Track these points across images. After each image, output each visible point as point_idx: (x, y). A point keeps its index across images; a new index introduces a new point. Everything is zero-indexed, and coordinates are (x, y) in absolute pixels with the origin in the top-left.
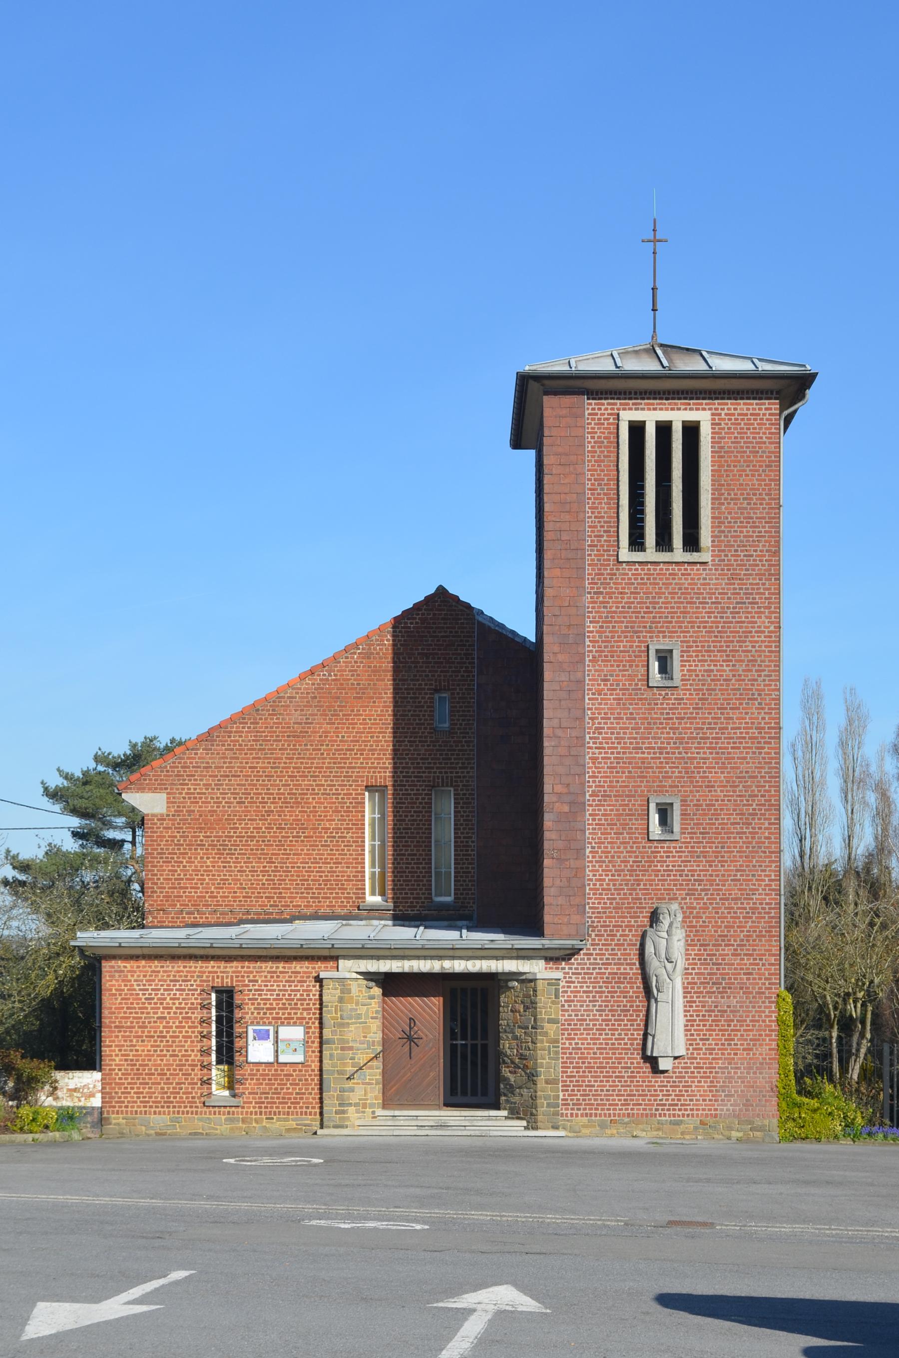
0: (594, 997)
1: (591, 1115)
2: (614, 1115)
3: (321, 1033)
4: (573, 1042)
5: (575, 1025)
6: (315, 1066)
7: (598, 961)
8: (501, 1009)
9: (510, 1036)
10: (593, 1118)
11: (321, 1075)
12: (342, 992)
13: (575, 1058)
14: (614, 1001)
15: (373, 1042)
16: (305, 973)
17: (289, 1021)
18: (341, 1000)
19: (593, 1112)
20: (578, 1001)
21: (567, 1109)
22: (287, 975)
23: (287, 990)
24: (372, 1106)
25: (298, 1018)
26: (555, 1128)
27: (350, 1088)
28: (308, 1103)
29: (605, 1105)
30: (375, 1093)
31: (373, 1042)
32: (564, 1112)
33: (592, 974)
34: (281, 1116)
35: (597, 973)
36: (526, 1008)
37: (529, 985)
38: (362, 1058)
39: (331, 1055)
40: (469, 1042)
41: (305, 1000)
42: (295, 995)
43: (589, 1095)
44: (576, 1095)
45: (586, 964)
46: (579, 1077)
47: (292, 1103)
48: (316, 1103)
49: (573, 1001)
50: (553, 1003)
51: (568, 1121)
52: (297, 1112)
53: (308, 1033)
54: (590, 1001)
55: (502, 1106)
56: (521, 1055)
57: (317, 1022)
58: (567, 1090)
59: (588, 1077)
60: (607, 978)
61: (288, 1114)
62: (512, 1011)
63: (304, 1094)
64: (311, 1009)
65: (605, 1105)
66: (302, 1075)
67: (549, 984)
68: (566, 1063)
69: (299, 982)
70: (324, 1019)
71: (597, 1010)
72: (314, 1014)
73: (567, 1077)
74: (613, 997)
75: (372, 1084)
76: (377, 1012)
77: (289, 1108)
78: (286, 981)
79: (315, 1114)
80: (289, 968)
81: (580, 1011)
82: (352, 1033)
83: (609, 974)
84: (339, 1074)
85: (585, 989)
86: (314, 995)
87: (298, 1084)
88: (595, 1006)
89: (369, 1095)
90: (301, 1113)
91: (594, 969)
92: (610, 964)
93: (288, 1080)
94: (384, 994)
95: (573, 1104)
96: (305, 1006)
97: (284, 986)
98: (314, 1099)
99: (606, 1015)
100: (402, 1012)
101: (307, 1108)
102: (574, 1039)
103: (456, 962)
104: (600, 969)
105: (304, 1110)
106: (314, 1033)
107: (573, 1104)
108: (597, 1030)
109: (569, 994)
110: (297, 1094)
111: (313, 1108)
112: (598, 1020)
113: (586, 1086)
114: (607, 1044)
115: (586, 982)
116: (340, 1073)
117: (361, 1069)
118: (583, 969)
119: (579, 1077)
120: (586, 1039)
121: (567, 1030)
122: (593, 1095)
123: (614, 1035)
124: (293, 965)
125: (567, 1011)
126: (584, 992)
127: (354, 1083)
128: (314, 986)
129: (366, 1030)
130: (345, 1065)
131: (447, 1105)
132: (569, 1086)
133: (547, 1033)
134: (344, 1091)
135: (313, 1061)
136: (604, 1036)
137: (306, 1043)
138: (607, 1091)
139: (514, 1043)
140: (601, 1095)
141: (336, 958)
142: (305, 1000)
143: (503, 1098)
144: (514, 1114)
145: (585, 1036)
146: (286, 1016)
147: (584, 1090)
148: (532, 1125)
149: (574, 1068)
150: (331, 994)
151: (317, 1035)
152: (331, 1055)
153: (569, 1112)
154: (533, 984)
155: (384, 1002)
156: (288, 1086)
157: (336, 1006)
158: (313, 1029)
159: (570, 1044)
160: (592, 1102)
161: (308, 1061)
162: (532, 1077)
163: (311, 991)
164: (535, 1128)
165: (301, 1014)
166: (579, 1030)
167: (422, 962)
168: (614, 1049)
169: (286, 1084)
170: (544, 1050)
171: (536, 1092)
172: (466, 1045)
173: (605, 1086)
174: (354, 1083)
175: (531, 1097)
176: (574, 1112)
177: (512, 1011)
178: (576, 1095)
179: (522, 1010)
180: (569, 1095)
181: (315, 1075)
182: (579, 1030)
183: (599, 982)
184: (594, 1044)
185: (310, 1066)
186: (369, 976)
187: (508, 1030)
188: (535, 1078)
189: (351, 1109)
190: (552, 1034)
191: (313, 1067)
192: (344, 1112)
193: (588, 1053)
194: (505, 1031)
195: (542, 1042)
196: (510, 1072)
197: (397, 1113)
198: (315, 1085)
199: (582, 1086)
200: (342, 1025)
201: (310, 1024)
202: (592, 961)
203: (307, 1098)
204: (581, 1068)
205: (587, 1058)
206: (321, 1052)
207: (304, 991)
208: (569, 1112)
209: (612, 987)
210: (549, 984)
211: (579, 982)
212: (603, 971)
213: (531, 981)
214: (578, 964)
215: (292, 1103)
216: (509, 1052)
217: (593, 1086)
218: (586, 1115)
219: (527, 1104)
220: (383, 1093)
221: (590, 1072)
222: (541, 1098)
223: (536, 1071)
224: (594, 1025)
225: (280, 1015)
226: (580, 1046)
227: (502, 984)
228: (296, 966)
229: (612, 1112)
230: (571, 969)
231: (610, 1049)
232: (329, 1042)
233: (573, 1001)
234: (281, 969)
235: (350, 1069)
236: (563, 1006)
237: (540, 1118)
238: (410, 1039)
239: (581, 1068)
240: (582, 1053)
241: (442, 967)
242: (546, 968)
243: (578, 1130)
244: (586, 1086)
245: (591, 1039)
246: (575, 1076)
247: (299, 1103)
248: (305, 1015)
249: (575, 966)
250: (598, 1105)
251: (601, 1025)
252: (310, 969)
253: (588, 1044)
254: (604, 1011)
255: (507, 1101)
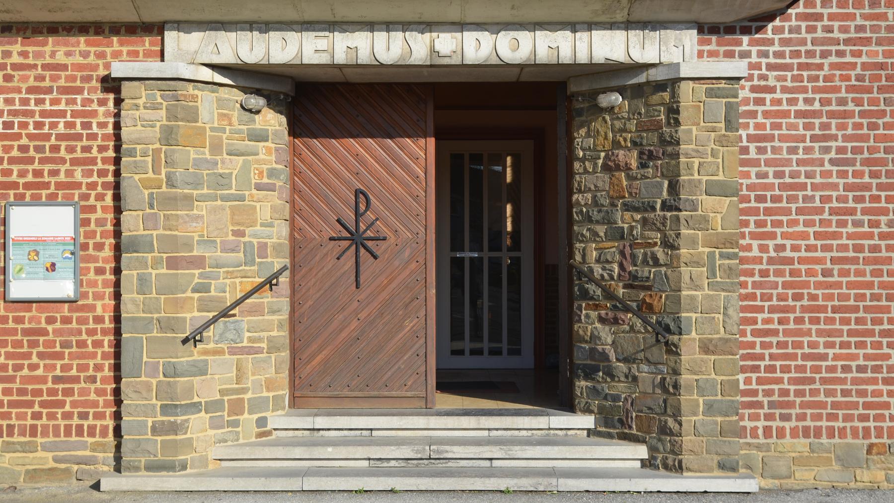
0: (825, 126)
1: (818, 433)
2: (879, 432)
3: (117, 223)
4: (771, 243)
5: (776, 199)
6: (103, 307)
7: (836, 34)
8: (577, 165)
9: (601, 230)
10: (824, 440)
11: (118, 332)
12: (172, 115)
13: (775, 286)
14: (877, 139)
15: (263, 247)
16: (79, 67)
17: (37, 193)
18: (168, 137)
19: (824, 423)
20: (782, 138)
21: (754, 417)
22: (32, 73)
23: (31, 114)
24: (257, 405)
25: (60, 186)
26: (728, 467)
27: (194, 364)
28: (85, 404)
29: (855, 406)
30: (269, 373)
31: (263, 247)
32: (749, 424)
33: (820, 67)
34: (16, 439)
35: (833, 66)
36: (646, 158)
37: (655, 98)
38: (228, 288)
39: (143, 281)
40: (486, 254)
41: (79, 137)
42: (53, 126)
43: (812, 381)
44: (780, 381)
45: (803, 42)
46: (786, 333)
47: (43, 404)
48: (106, 404)
49: (771, 138)
50: (720, 141)
51: (758, 447)
52: (56, 428)
53: (86, 222)
54: (814, 138)
55: (581, 402)
56: (634, 277)
57: (110, 194)
58: (756, 369)
59: (809, 333)
60: (859, 78)
61: (33, 433)
62: (606, 168)
63: (76, 380)
64: (93, 161)
65: (855, 406)
66: (71, 332)
67: (710, 93)
68: (753, 297)
69: (64, 90)
70: (124, 184)
71: (832, 162)
72: (102, 173)
73: (755, 333)
74: (873, 126)
75: (259, 351)
76: (272, 173)
77: (37, 416)
78: (30, 90)
79: (104, 434)
80: (38, 55)
81: (788, 163)
82: (203, 222)
83: (865, 66)
84: (161, 329)
85: (801, 106)
86: (102, 125)
87: (59, 356)
88: (827, 150)
89: (251, 380)
90: (68, 429)
91: (825, 55)
92: (867, 41)
93: (33, 344)
94: (295, 130)
95: (771, 405)
96: (79, 154)
97: (25, 102)
98: (100, 392)
99: (857, 174)
100: (337, 175)
101: (84, 416)
102: (773, 236)
103: (470, 37)
104: (840, 54)
105: (76, 421)
106: (100, 222)
107: (771, 405)
108: (832, 211)
109: (760, 119)
110: (57, 380)
111: (99, 416)
112: (835, 186)
113: (805, 357)
114: (858, 249)
115: (804, 90)
116: (166, 325)
117: (225, 314)
118: (797, 54)
119: (786, 333)
120: (804, 236)
121: (755, 212)
122: (824, 381)
123: (877, 224)
124: (48, 49)
125: (755, 163)
126: (800, 114)
127: (206, 352)
128: (102, 102)
129: (243, 217)
130: (179, 305)
131: (451, 382)
132: (761, 357)
133: (705, 219)
134: (176, 375)
135: (98, 296)
136: (850, 229)
137: (80, 249)
138: (860, 369)
139: (612, 248)
140: (843, 381)
141: (157, 29)
142: (79, 137)
143: (582, 384)
144: (614, 425)
145: (800, 228)
146: (30, 178)
147: (799, 369)
148: (666, 458)
149: (772, 310)
150: (143, 120)
151: (110, 227)
152: (143, 281)
153: (761, 424)
154: (666, 96)
155: (295, 152)
156: (35, 359)
157: (157, 152)
158: (99, 214)
159: (763, 249)
160: (822, 398)
161: (85, 295)
162: (666, 334)
163: (94, 114)
164: (678, 468)
165: (69, 173)
166: (787, 212)
167: (381, 37)
168: (876, 261)
169: (28, 356)
170: (698, 264)
171: (676, 372)
172: (480, 259)
173: (854, 357)
174: (206, 352)
175: (662, 384)
176: (774, 424)
177: (606, 168)
178: (780, 381)
179: (634, 164)
180: (760, 381)
181: (104, 332)
182: (787, 212)
183: (837, 89)
184: (826, 248)
185: (92, 308)
186: (231, 70)
187: (596, 215)
188: (675, 338)
189: (198, 422)
190: (717, 221)
191: (99, 311)
192: (174, 428)
193: (810, 273)
194: (589, 219)
195: (693, 243)
196: (602, 320)
197: (321, 422)
198: (105, 356)
199: (794, 357)
200: (171, 202)
201: (92, 201)
202: (820, 34)
203: (83, 392)
204: (792, 309)
205: (806, 285)
206: (117, 271)
207: (75, 114)
208: (761, 424)
209: (873, 102)
210: (710, 93)
211: (784, 90)
212: (849, 59)
213: (661, 86)
214: (784, 42)
215: (43, 404)
216: (598, 270)
217: (824, 357)
218: (806, 432)
219: (649, 402)
220: (293, 369)
221: (816, 321)
222: (690, 390)
223: (677, 320)
224: (825, 199)
225: (14, 177)
226: (788, 253)
227: (580, 104)
228: (55, 50)
229: (871, 424)
230: (765, 54)
231: (866, 261)
232: (136, 245)
233: (771, 138)
234: (16, 59)
235: (193, 316)
236: (745, 150)
237: (688, 440)
238: (356, 240)
239: (792, 309)
240: (792, 273)
241: (433, 51)
242: (700, 54)
243: (784, 471)
244: (805, 357)
245: (817, 235)
246: (775, 333)
247: (62, 404)
248: (78, 176)
249: (777, 48)
250: (835, 405)
251: (844, 199)
252: (92, 59)
253: (809, 248)
254: (852, 163)
255: (594, 392)
